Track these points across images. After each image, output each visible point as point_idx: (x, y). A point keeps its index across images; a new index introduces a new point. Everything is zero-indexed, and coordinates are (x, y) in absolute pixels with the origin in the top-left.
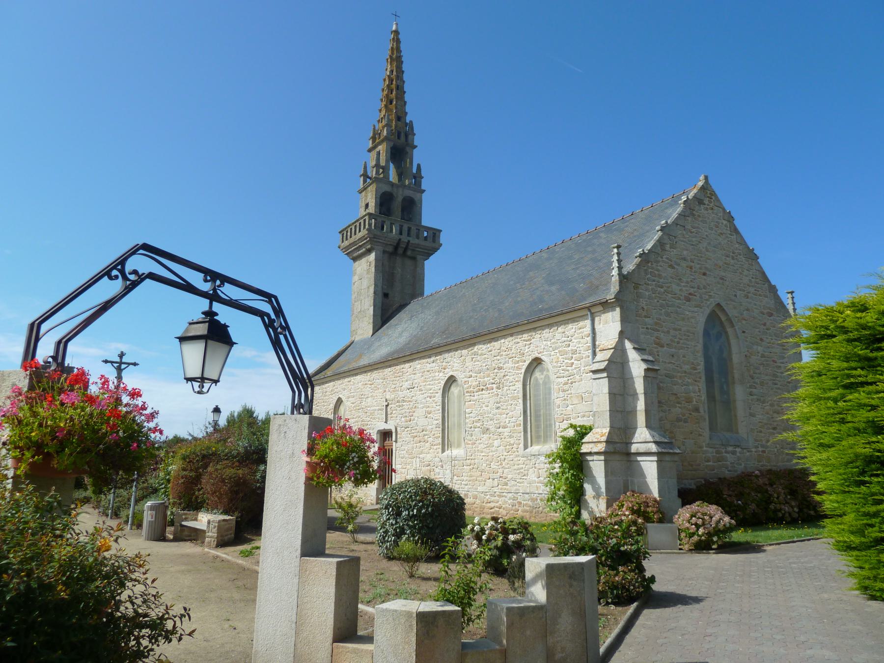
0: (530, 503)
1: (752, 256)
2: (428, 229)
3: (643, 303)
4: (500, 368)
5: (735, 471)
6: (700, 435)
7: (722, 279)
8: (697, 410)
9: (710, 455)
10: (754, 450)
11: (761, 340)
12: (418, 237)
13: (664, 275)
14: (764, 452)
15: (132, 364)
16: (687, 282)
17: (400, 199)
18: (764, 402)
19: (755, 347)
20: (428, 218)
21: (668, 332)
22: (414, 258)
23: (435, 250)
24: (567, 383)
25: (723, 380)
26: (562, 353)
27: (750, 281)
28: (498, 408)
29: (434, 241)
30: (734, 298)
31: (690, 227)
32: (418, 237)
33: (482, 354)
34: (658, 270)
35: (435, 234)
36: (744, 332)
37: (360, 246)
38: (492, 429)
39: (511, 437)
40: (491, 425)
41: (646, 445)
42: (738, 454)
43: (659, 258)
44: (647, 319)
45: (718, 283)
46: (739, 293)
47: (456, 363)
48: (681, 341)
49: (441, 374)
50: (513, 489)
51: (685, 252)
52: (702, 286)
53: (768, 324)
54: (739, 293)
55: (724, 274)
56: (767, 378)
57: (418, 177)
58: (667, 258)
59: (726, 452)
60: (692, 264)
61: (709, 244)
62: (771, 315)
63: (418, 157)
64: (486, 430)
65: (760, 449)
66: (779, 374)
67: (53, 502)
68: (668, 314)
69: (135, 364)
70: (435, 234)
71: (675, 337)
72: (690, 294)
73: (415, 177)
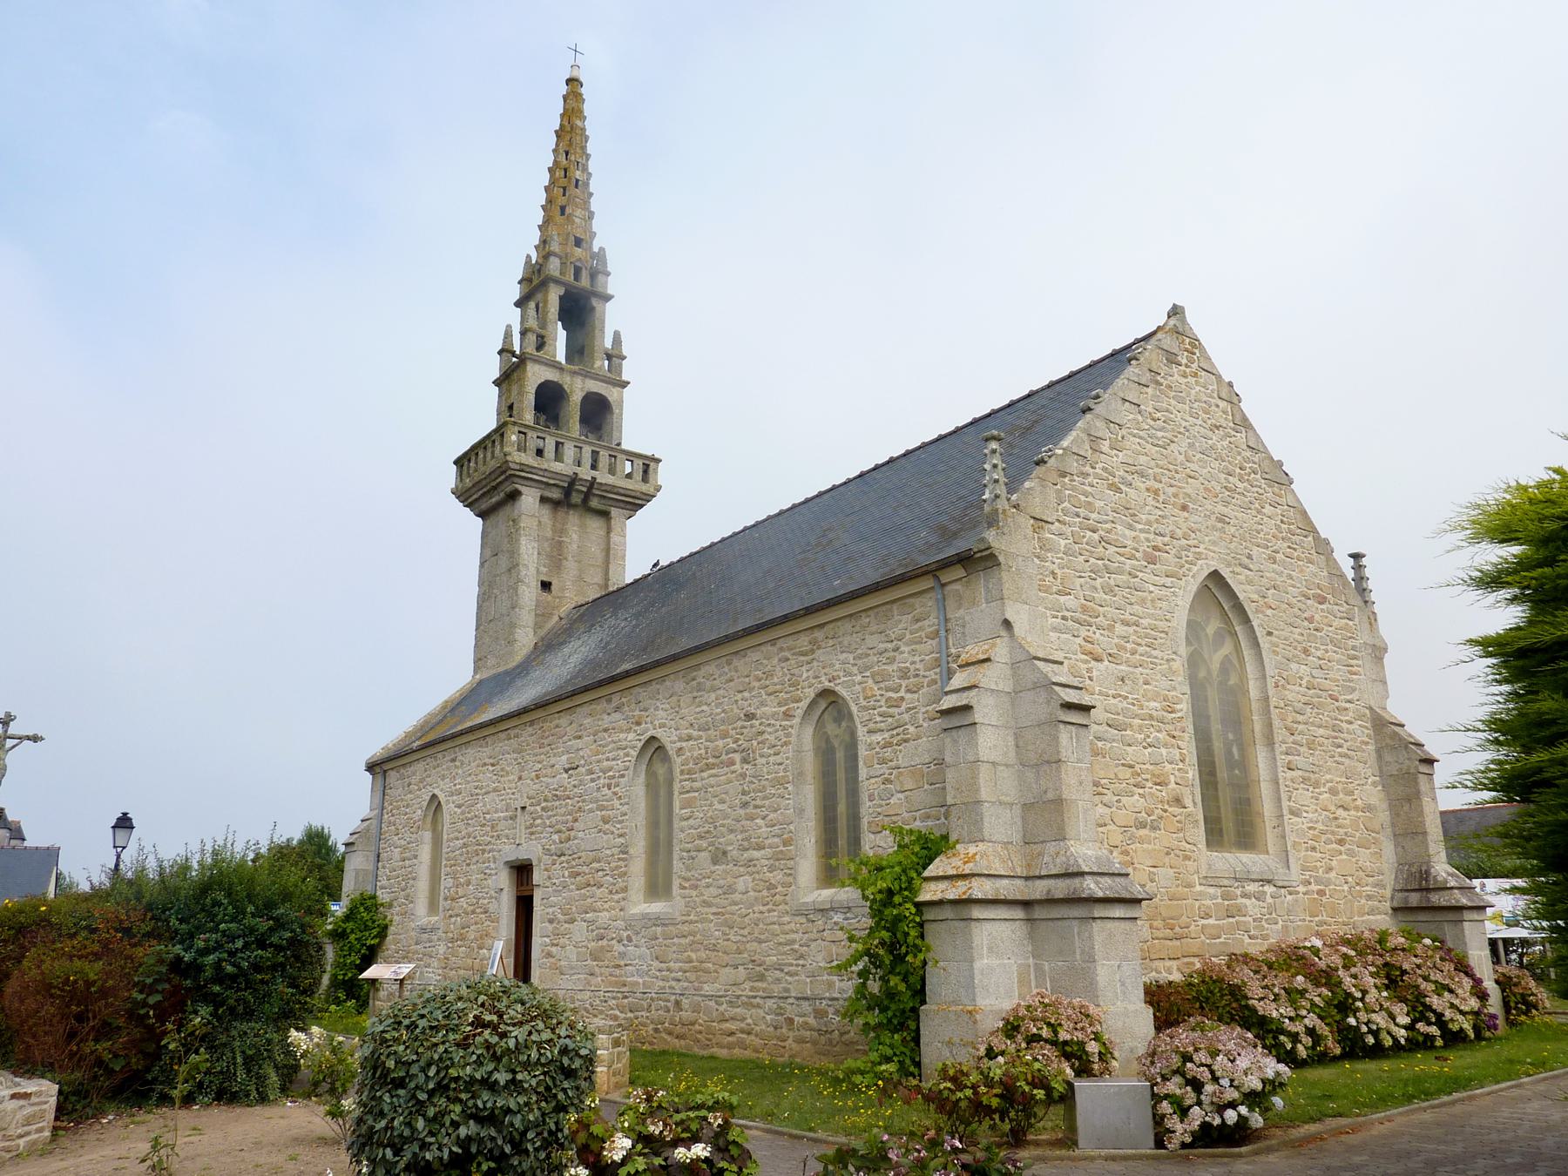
0: (811, 1021)
1: (1279, 478)
2: (632, 456)
3: (1054, 561)
4: (750, 717)
5: (1265, 937)
6: (1187, 858)
7: (1220, 520)
8: (1178, 801)
9: (1208, 902)
10: (1301, 889)
11: (1306, 651)
12: (612, 471)
13: (1099, 504)
14: (1321, 893)
15: (28, 738)
16: (1149, 523)
17: (576, 398)
18: (1316, 785)
19: (1294, 666)
20: (636, 430)
21: (1111, 628)
22: (605, 514)
23: (648, 497)
24: (889, 745)
25: (1231, 736)
26: (880, 678)
27: (1278, 527)
28: (745, 805)
29: (645, 479)
30: (1247, 561)
31: (1150, 409)
32: (612, 471)
33: (713, 689)
34: (1086, 494)
35: (648, 465)
36: (1270, 634)
37: (494, 488)
38: (734, 853)
39: (772, 869)
40: (731, 842)
41: (1068, 881)
42: (1269, 900)
43: (1088, 469)
44: (1062, 599)
45: (1214, 528)
46: (1255, 551)
47: (667, 713)
48: (1141, 649)
49: (631, 736)
50: (777, 989)
51: (1143, 459)
52: (1179, 533)
53: (1317, 617)
54: (1255, 551)
55: (1225, 511)
56: (1321, 731)
57: (615, 356)
58: (1104, 469)
59: (1244, 895)
60: (1158, 485)
61: (1191, 445)
62: (1322, 601)
63: (614, 319)
64: (719, 856)
65: (1314, 887)
66: (1344, 725)
67: (196, 979)
68: (1109, 590)
69: (35, 739)
70: (648, 465)
71: (1126, 638)
72: (1155, 548)
73: (609, 357)
